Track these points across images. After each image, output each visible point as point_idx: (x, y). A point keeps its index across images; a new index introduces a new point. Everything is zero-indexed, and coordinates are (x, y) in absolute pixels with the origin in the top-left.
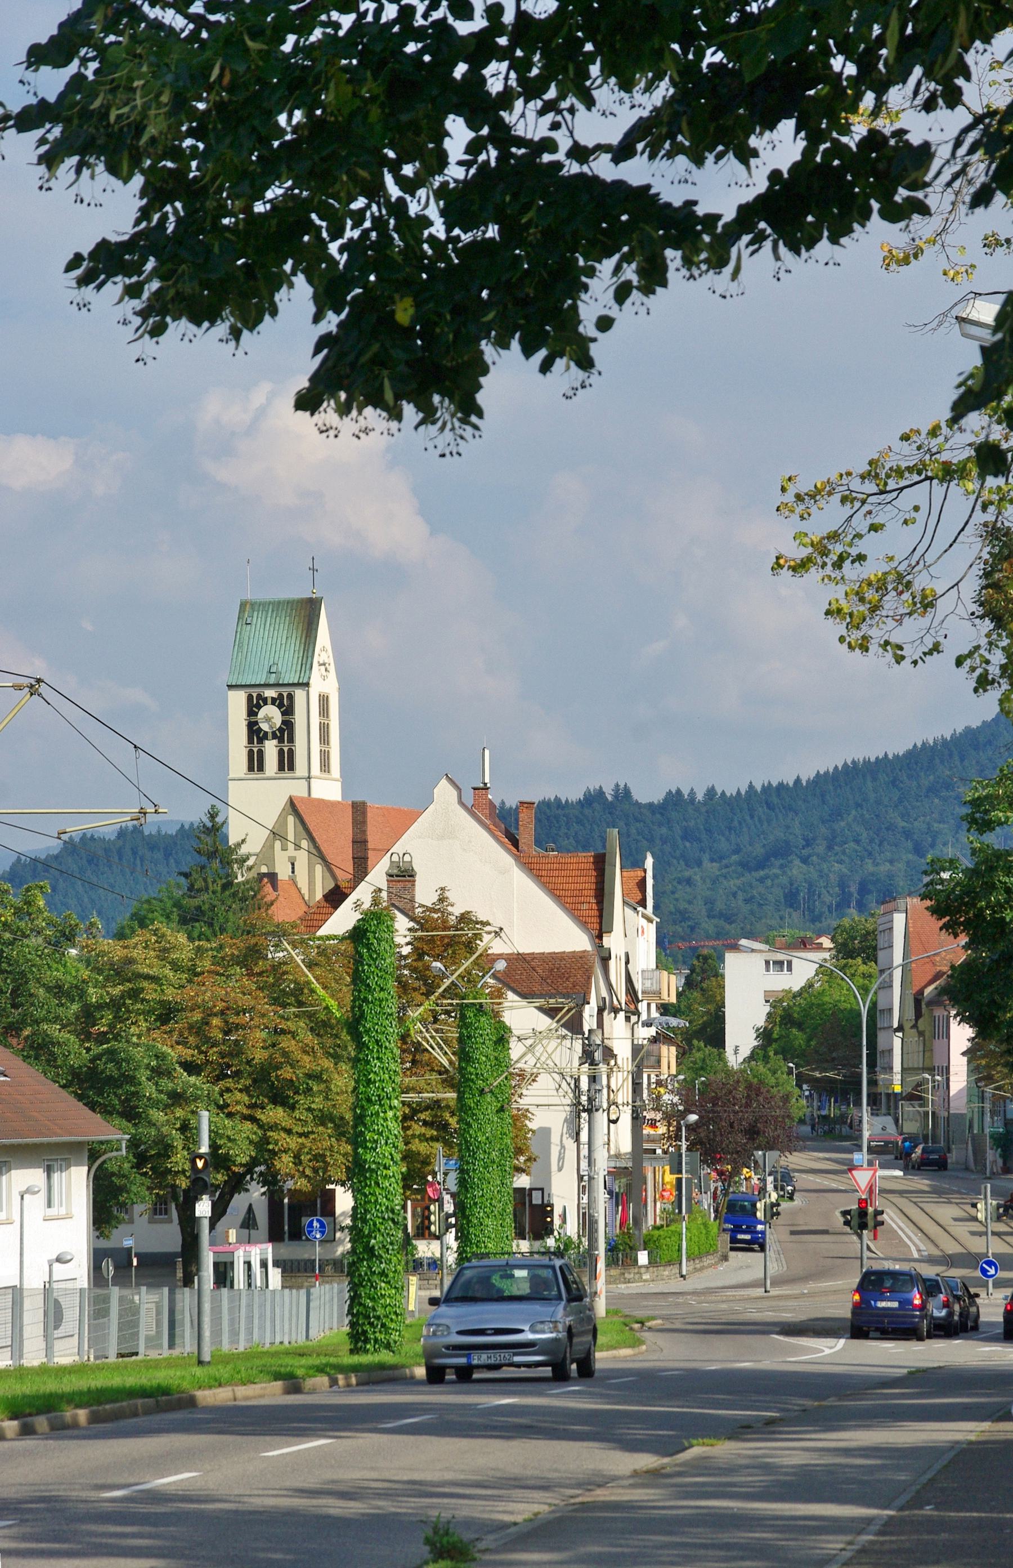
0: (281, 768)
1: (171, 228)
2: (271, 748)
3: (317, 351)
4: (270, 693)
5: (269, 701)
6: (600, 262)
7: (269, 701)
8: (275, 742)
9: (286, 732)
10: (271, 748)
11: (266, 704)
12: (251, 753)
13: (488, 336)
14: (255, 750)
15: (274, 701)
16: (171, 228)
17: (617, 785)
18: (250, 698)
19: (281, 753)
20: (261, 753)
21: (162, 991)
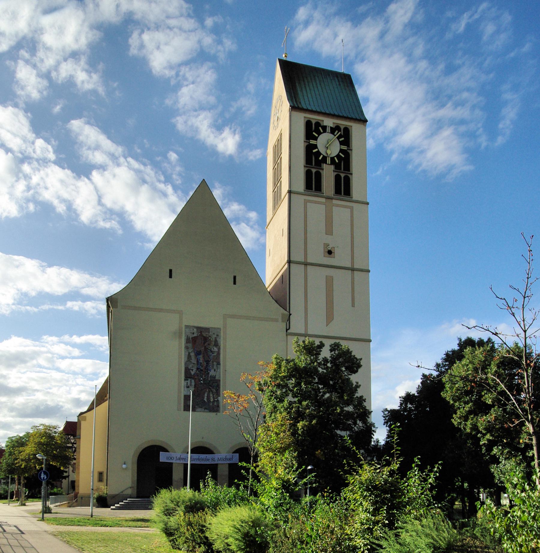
0: (338, 191)
1: (400, 448)
2: (328, 174)
3: (63, 201)
4: (329, 122)
5: (328, 130)
6: (190, 488)
7: (328, 130)
8: (332, 167)
9: (343, 162)
10: (328, 174)
11: (325, 131)
12: (308, 174)
13: (56, 443)
14: (314, 171)
15: (333, 130)
16: (400, 448)
17: (375, 432)
18: (308, 124)
19: (337, 178)
20: (319, 176)
21: (269, 507)
